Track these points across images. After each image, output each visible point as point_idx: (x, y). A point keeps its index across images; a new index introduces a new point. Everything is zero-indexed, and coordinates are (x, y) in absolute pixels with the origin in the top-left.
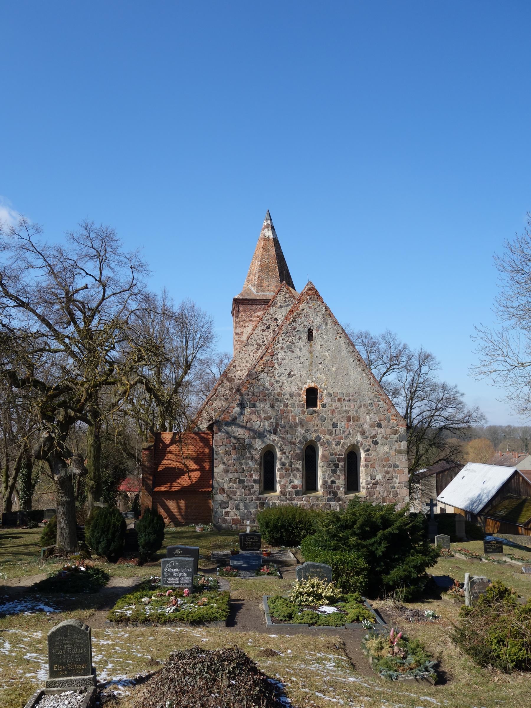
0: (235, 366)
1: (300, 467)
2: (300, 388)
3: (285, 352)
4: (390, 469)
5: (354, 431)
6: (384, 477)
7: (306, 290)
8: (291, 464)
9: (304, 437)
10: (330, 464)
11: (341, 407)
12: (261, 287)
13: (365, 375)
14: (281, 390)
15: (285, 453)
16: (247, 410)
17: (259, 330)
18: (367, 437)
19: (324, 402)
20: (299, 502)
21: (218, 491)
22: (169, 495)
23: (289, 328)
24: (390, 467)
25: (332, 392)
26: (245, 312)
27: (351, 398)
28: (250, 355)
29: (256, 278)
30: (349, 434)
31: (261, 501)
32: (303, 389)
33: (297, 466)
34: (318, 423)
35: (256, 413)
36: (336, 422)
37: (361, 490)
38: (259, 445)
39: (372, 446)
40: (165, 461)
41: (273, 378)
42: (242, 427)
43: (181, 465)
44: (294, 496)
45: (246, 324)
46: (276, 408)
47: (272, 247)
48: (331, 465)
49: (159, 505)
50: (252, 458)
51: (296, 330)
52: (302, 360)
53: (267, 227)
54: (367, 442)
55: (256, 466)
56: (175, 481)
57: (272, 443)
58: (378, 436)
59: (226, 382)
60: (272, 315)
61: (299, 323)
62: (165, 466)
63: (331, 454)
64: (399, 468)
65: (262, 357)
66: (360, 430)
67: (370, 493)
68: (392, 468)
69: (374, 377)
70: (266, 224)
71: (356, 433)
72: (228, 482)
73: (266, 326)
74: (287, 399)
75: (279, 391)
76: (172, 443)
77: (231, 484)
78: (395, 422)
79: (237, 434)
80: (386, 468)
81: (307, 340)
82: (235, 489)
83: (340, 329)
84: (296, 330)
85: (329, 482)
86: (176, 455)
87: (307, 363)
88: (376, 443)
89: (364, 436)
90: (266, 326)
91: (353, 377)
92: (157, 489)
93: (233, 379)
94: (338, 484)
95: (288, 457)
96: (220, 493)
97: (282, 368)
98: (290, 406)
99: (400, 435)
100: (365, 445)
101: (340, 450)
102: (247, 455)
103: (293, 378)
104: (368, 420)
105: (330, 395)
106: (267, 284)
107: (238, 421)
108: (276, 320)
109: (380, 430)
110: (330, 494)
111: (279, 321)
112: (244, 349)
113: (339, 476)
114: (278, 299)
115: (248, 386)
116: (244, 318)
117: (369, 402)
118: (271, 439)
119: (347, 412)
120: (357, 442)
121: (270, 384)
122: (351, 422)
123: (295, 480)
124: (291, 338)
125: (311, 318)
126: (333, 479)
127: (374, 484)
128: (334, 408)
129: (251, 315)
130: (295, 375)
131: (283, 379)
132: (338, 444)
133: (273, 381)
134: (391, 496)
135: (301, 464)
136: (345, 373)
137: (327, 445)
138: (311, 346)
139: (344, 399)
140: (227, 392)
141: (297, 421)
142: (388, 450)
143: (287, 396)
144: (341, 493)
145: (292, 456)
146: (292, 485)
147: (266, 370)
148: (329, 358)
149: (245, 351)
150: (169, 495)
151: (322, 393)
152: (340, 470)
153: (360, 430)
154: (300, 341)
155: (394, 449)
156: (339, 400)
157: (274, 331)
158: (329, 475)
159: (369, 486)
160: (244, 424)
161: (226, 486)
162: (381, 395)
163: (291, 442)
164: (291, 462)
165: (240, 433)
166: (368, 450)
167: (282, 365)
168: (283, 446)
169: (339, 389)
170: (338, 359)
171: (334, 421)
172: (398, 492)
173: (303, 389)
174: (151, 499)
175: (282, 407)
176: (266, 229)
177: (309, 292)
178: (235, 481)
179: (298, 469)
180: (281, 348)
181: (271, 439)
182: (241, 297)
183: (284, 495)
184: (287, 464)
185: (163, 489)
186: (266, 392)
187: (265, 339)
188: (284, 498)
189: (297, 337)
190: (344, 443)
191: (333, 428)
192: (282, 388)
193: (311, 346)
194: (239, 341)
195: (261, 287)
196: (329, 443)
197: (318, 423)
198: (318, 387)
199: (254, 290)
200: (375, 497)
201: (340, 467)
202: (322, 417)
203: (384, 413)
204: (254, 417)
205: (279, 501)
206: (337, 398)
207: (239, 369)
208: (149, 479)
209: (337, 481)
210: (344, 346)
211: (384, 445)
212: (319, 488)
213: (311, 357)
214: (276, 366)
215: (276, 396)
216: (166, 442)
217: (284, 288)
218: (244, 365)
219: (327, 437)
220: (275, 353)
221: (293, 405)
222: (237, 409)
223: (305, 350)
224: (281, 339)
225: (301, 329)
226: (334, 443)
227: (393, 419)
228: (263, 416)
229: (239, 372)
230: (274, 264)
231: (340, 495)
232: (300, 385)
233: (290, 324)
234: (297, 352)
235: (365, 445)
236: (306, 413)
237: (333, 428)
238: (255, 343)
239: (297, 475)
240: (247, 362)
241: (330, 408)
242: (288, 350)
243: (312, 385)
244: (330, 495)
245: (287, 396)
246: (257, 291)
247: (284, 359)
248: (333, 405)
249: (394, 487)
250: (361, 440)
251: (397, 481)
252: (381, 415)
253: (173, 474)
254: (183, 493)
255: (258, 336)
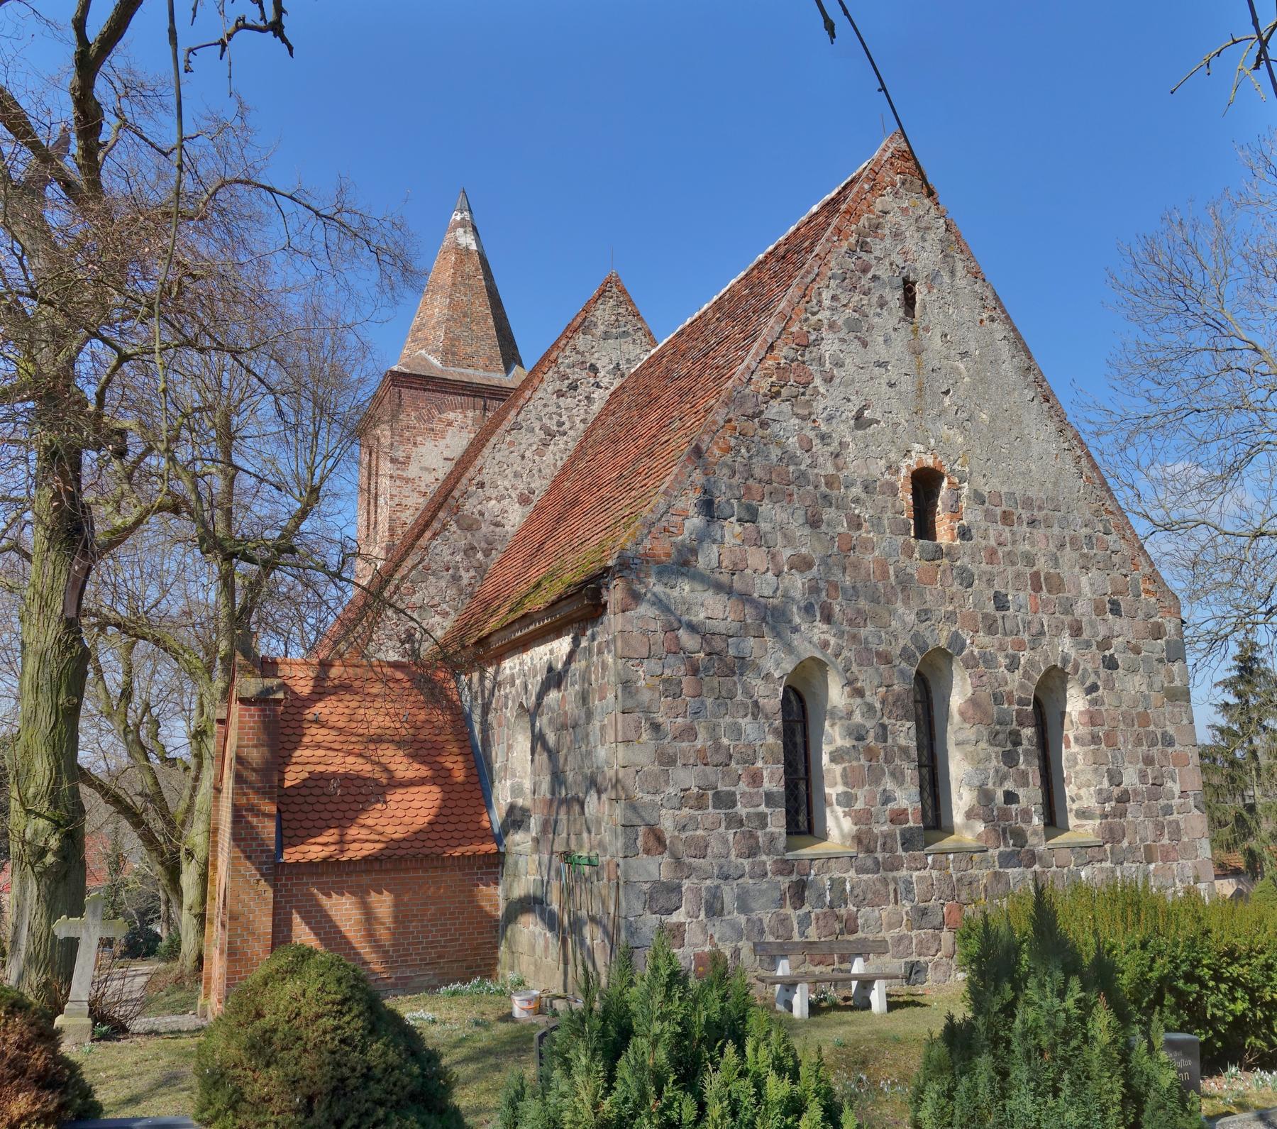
0: (481, 485)
1: (913, 744)
2: (893, 468)
3: (842, 340)
4: (1155, 752)
5: (1054, 622)
6: (1143, 776)
7: (888, 154)
8: (883, 730)
9: (916, 637)
10: (997, 733)
11: (1014, 542)
12: (454, 354)
13: (1066, 445)
14: (838, 469)
15: (859, 693)
16: (732, 530)
17: (550, 389)
18: (1088, 645)
19: (964, 522)
20: (916, 874)
21: (640, 842)
22: (336, 872)
23: (850, 263)
24: (1153, 744)
25: (985, 490)
26: (417, 408)
27: (1039, 515)
28: (523, 457)
29: (441, 333)
30: (1042, 633)
31: (794, 877)
32: (904, 472)
33: (902, 741)
34: (954, 589)
35: (759, 540)
36: (1003, 591)
37: (1072, 821)
38: (777, 664)
39: (1103, 672)
40: (308, 753)
41: (811, 424)
42: (719, 587)
43: (368, 767)
44: (900, 852)
45: (419, 439)
46: (824, 528)
47: (477, 270)
48: (1001, 736)
49: (296, 918)
50: (756, 710)
51: (870, 275)
52: (893, 374)
53: (462, 224)
54: (1089, 661)
55: (770, 739)
56: (352, 820)
57: (818, 655)
58: (1114, 642)
59: (454, 528)
60: (582, 354)
61: (877, 253)
62: (309, 768)
63: (997, 699)
64: (1177, 747)
65: (771, 347)
66: (1068, 619)
67: (1111, 831)
68: (1160, 746)
69: (1089, 455)
70: (458, 218)
71: (1059, 630)
72: (676, 802)
73: (567, 382)
74: (857, 500)
75: (830, 470)
76: (320, 692)
77: (686, 811)
78: (1153, 600)
79: (702, 616)
80: (1145, 748)
81: (901, 314)
82: (700, 832)
83: (988, 294)
84: (870, 275)
85: (1000, 796)
86: (341, 731)
87: (907, 385)
88: (1111, 664)
89: (1080, 639)
90: (567, 382)
91: (1036, 450)
92: (291, 855)
93: (477, 521)
94: (1023, 802)
95: (870, 708)
96: (647, 852)
97: (837, 392)
98: (866, 525)
99: (1168, 642)
100: (1085, 670)
101: (1022, 686)
102: (739, 697)
103: (870, 430)
104: (1086, 589)
105: (979, 498)
106: (469, 350)
107: (701, 563)
108: (594, 369)
109: (1118, 624)
110: (1005, 838)
111: (602, 373)
112: (508, 439)
113: (1024, 775)
114: (598, 313)
115: (733, 442)
116: (414, 422)
117: (1084, 531)
118: (815, 639)
119: (1030, 560)
120: (1065, 660)
121: (800, 441)
122: (1044, 594)
123: (898, 794)
124: (856, 298)
125: (911, 242)
126: (1009, 785)
127: (1119, 800)
128: (993, 543)
129: (430, 418)
130: (878, 422)
131: (842, 430)
132: (1013, 665)
133: (812, 435)
134: (1165, 841)
135: (913, 731)
136: (1014, 434)
137: (982, 668)
138: (915, 332)
139: (1019, 518)
140: (458, 558)
141: (893, 578)
142: (1144, 688)
143: (856, 491)
144: (1035, 833)
145: (883, 702)
146: (892, 811)
147: (785, 392)
148: (967, 379)
149: (512, 443)
150: (336, 872)
151: (955, 488)
152: (1026, 752)
153: (1068, 619)
154: (885, 313)
155: (1157, 686)
156: (1007, 518)
157: (588, 398)
158: (997, 771)
159: (1108, 807)
160: (725, 578)
161: (667, 824)
162: (1111, 513)
163: (878, 654)
164: (884, 727)
165: (711, 609)
166: (1093, 688)
167: (836, 381)
168: (854, 668)
169: (1003, 483)
170: (994, 387)
171: (997, 588)
172: (1182, 825)
173: (904, 472)
174: (270, 894)
175: (843, 528)
176: (460, 230)
177: (898, 163)
178: (701, 797)
179: (904, 751)
180: (831, 327)
181: (815, 639)
182: (407, 371)
183: (870, 851)
184: (872, 733)
185: (314, 851)
186: (791, 468)
187: (564, 418)
188: (869, 863)
189: (875, 299)
190: (1031, 662)
191: (998, 609)
192: (840, 461)
193: (915, 332)
194: (400, 477)
195: (454, 354)
196: (989, 661)
197: (954, 589)
198: (947, 469)
199: (436, 362)
200: (1125, 844)
201: (1025, 742)
202: (963, 570)
203: (1124, 571)
204: (757, 558)
205: (852, 873)
206: (998, 511)
207: (494, 493)
208: (258, 813)
209: (1021, 792)
210: (1005, 350)
211: (1133, 670)
212: (958, 818)
213: (919, 367)
214: (818, 381)
215: (823, 488)
216: (297, 689)
217: (615, 290)
218: (506, 483)
219: (983, 638)
220: (812, 338)
221: (877, 523)
222: (696, 521)
223: (900, 341)
224: (826, 295)
225: (883, 272)
226: (1003, 661)
227: (1148, 592)
228: (786, 553)
229: (493, 502)
230: (482, 307)
231: (1032, 840)
232: (893, 456)
233: (851, 252)
234: (878, 349)
235: (1085, 670)
236: (917, 555)
237: (998, 609)
238: (537, 425)
239: (902, 774)
240: (516, 475)
241: (984, 543)
242: (852, 335)
243: (929, 461)
244: (1007, 845)
245: (856, 491)
246: (444, 362)
247: (839, 364)
248: (991, 532)
249: (1168, 810)
250: (1073, 653)
251: (1176, 789)
252: (1116, 574)
253: (344, 799)
254: (392, 863)
255: (545, 406)
